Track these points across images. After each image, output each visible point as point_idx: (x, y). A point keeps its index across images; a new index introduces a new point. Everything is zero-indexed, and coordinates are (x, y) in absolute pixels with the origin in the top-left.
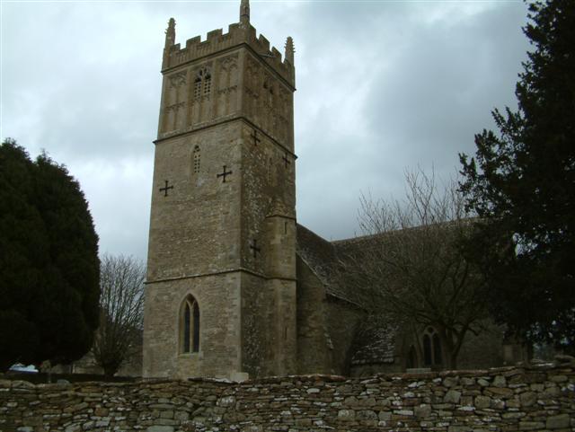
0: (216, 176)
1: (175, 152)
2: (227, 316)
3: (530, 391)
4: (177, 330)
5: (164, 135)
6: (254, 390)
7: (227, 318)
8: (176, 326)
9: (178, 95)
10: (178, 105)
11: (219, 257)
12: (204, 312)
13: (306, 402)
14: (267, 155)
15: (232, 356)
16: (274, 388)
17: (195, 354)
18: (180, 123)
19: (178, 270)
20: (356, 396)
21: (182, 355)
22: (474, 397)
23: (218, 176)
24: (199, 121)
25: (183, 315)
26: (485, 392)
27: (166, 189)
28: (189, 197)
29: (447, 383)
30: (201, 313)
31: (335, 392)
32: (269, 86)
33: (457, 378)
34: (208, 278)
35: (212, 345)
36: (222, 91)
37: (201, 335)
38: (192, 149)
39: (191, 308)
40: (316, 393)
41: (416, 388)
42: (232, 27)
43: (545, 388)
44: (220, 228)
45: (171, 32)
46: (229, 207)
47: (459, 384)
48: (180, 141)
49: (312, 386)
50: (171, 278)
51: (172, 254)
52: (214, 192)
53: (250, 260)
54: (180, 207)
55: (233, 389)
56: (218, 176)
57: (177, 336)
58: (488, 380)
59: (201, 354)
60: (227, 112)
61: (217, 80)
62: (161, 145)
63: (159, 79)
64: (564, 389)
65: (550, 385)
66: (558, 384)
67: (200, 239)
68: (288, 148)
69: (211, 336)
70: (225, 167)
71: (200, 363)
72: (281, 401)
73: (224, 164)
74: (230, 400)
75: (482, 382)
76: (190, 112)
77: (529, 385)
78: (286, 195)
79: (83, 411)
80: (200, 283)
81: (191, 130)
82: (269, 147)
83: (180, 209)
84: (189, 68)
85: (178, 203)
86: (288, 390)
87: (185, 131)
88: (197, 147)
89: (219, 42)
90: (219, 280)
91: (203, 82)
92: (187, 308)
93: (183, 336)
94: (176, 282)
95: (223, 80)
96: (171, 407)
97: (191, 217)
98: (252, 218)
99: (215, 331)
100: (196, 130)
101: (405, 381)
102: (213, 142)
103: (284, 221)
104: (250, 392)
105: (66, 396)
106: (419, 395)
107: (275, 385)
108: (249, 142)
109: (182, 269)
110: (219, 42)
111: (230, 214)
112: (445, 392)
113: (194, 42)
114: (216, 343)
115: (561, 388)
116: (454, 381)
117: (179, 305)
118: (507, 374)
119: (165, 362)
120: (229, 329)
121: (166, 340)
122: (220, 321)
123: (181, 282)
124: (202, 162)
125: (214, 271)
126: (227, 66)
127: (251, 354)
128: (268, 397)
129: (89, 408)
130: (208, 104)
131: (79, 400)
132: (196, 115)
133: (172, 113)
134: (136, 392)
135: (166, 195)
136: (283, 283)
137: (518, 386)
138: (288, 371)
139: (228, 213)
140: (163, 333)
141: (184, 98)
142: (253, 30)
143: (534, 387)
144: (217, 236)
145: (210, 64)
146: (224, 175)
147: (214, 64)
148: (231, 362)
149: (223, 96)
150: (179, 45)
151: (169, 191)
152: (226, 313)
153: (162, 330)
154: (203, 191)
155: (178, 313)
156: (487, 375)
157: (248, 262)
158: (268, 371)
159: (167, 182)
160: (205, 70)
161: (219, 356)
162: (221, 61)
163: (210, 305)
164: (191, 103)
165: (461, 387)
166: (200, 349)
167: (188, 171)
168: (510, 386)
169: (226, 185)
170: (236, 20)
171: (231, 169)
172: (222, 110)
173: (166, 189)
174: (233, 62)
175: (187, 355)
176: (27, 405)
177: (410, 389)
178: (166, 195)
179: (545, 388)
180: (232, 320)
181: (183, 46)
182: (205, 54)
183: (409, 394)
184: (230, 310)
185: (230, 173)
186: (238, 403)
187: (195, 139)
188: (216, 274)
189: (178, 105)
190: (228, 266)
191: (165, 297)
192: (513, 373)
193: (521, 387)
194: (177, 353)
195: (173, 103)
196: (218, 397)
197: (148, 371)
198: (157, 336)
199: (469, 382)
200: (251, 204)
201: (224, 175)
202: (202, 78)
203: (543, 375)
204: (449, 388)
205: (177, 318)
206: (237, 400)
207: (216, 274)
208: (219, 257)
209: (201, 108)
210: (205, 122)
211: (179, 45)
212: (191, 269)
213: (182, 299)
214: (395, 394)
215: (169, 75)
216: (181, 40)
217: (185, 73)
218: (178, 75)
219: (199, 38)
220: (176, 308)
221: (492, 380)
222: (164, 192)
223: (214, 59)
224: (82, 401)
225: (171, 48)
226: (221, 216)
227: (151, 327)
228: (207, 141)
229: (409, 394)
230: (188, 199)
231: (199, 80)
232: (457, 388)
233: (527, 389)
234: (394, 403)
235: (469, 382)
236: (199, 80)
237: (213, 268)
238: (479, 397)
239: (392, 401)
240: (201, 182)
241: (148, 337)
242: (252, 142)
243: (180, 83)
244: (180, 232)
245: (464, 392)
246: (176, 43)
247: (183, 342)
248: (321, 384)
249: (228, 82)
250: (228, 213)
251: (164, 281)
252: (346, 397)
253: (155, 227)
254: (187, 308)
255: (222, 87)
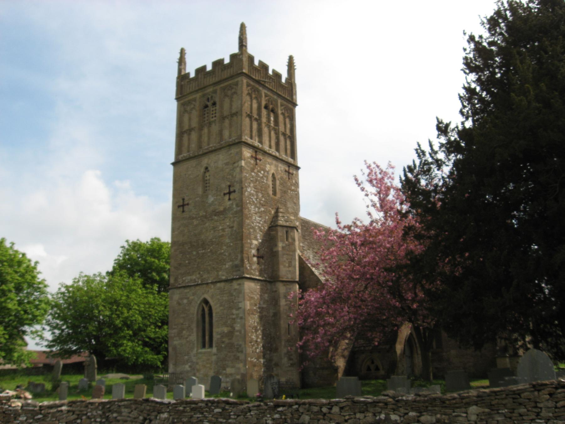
0: (222, 194)
1: (190, 172)
2: (234, 317)
3: (355, 418)
4: (195, 330)
5: (180, 157)
6: (181, 408)
7: (234, 319)
8: (194, 326)
9: (190, 119)
10: (190, 130)
11: (227, 266)
12: (216, 313)
13: (213, 419)
14: (268, 172)
15: (239, 352)
16: (193, 408)
17: (209, 350)
18: (193, 146)
19: (194, 277)
20: (244, 416)
21: (200, 351)
22: (319, 420)
23: (225, 194)
24: (209, 144)
25: (200, 316)
26: (326, 417)
27: (183, 206)
28: (202, 213)
29: (301, 410)
30: (214, 315)
31: (231, 412)
32: (271, 106)
33: (307, 406)
34: (218, 285)
35: (223, 342)
36: (226, 117)
37: (214, 334)
38: (203, 170)
39: (206, 310)
40: (220, 413)
41: (282, 411)
42: (233, 57)
43: (365, 417)
44: (227, 241)
45: (182, 61)
46: (234, 221)
47: (308, 411)
48: (193, 163)
49: (217, 407)
50: (190, 284)
51: (189, 263)
52: (222, 209)
53: (254, 267)
54: (195, 222)
55: (168, 407)
56: (225, 194)
57: (195, 334)
58: (329, 408)
59: (214, 350)
60: (230, 137)
61: (222, 107)
62: (185, 165)
63: (173, 106)
64: (378, 418)
65: (368, 415)
66: (375, 415)
67: (211, 251)
68: (290, 160)
69: (223, 335)
70: (230, 186)
71: (214, 358)
72: (198, 417)
73: (229, 183)
74: (165, 415)
75: (324, 410)
76: (200, 137)
77: (355, 414)
78: (289, 205)
79: (74, 422)
80: (212, 289)
81: (201, 153)
82: (270, 164)
83: (195, 223)
84: (198, 95)
85: (193, 218)
86: (202, 409)
87: (196, 154)
88: (207, 168)
89: (222, 70)
90: (227, 286)
91: (211, 108)
92: (203, 310)
93: (200, 334)
94: (193, 288)
95: (226, 105)
96: (129, 419)
97: (204, 231)
98: (255, 230)
99: (226, 330)
100: (206, 153)
101: (277, 406)
102: (220, 164)
103: (285, 229)
104: (179, 410)
105: (61, 411)
106: (283, 417)
107: (193, 406)
108: (250, 163)
109: (198, 276)
110: (222, 70)
111: (234, 229)
112: (300, 416)
113: (201, 71)
114: (226, 340)
115: (376, 416)
116: (305, 409)
117: (196, 308)
118: (342, 405)
119: (186, 357)
120: (237, 328)
121: (187, 338)
122: (229, 322)
123: (198, 288)
124: (211, 181)
125: (224, 278)
126: (229, 93)
127: (256, 349)
128: (189, 414)
129: (77, 419)
130: (215, 128)
131: (71, 413)
132: (205, 138)
133: (185, 137)
134: (109, 408)
135: (183, 211)
136: (284, 285)
137: (347, 414)
138: (291, 362)
139: (232, 227)
140: (184, 332)
141: (195, 123)
142: (251, 59)
143: (358, 415)
144: (224, 247)
145: (215, 92)
146: (230, 193)
147: (218, 92)
148: (239, 357)
149: (227, 121)
150: (189, 74)
151: (186, 208)
152: (233, 314)
153: (183, 329)
154: (212, 208)
155: (195, 315)
156: (329, 404)
157: (252, 269)
158: (273, 362)
159: (183, 199)
160: (212, 97)
161: (229, 352)
162: (224, 89)
163: (221, 308)
164: (201, 129)
165: (310, 413)
166: (214, 345)
167: (200, 191)
168: (342, 414)
169: (231, 202)
170: (236, 50)
171: (235, 188)
172: (226, 133)
173: (183, 206)
174: (233, 91)
175: (204, 350)
176: (33, 418)
177: (278, 412)
178: (183, 211)
179: (365, 417)
180: (239, 320)
181: (192, 75)
182: (211, 83)
183: (277, 416)
184: (237, 312)
185: (234, 191)
186: (171, 418)
187: (205, 161)
188: (226, 281)
189: (190, 130)
190: (235, 273)
191: (185, 301)
192: (344, 404)
193: (349, 415)
194: (195, 349)
195: (186, 127)
196: (159, 413)
197: (173, 365)
198: (179, 335)
199: (315, 409)
200: (254, 218)
201: (230, 193)
202: (209, 104)
203: (365, 407)
204: (302, 413)
205: (195, 319)
206: (170, 415)
207: (226, 281)
208: (227, 266)
209: (209, 132)
210: (213, 145)
211: (189, 74)
212: (205, 276)
213: (199, 302)
214: (268, 416)
215: (182, 102)
216: (191, 70)
217: (195, 100)
218: (189, 102)
219: (204, 67)
220: (194, 310)
221: (331, 409)
222: (181, 209)
223: (218, 87)
224: (73, 414)
225: (182, 78)
226: (228, 230)
227: (174, 327)
228: (215, 162)
229: (277, 416)
230: (201, 214)
231: (206, 106)
232: (308, 413)
233: (352, 416)
234: (268, 422)
235: (315, 409)
236: (206, 106)
237: (223, 275)
238: (321, 421)
239: (266, 420)
240: (211, 199)
241: (173, 335)
242: (252, 162)
243: (192, 109)
244: (195, 244)
245: (312, 416)
246: (187, 72)
247: (200, 340)
248: (223, 405)
249: (231, 108)
250: (232, 227)
251: (184, 287)
252: (238, 416)
253: (175, 240)
254: (203, 310)
255: (226, 113)
